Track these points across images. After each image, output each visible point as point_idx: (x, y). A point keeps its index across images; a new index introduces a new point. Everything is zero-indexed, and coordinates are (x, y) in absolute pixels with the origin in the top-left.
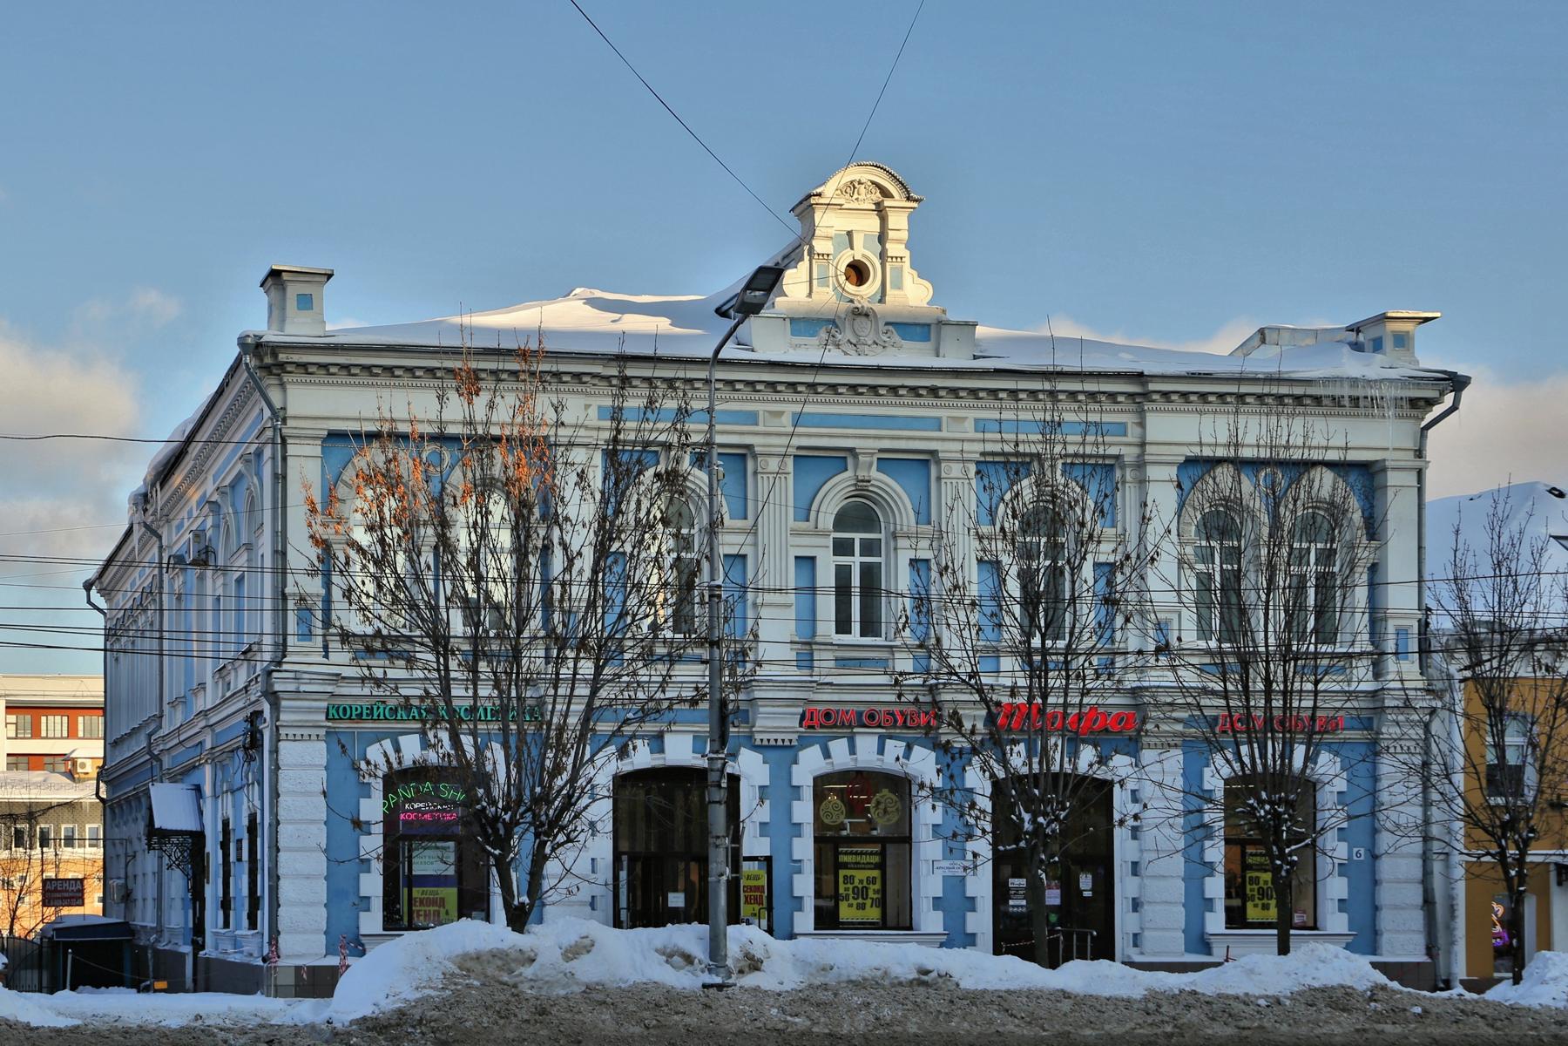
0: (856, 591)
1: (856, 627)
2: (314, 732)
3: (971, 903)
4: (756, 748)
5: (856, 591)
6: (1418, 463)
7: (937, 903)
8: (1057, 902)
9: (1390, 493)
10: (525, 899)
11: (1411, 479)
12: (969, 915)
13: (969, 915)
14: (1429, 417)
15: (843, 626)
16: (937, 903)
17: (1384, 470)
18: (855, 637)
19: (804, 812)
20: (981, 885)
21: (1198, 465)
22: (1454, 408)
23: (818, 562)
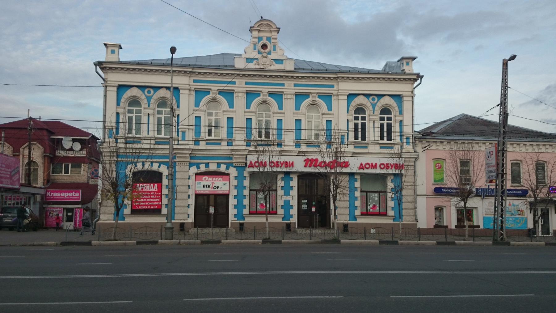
0: (360, 130)
1: (385, 138)
2: (186, 163)
3: (291, 207)
4: (234, 167)
5: (360, 130)
6: (412, 95)
7: (282, 207)
8: (166, 213)
9: (405, 102)
10: (15, 211)
11: (410, 99)
12: (291, 210)
13: (291, 210)
14: (415, 85)
15: (356, 138)
16: (282, 207)
17: (403, 97)
18: (385, 141)
19: (246, 183)
20: (294, 202)
21: (351, 96)
22: (420, 83)
23: (283, 120)
